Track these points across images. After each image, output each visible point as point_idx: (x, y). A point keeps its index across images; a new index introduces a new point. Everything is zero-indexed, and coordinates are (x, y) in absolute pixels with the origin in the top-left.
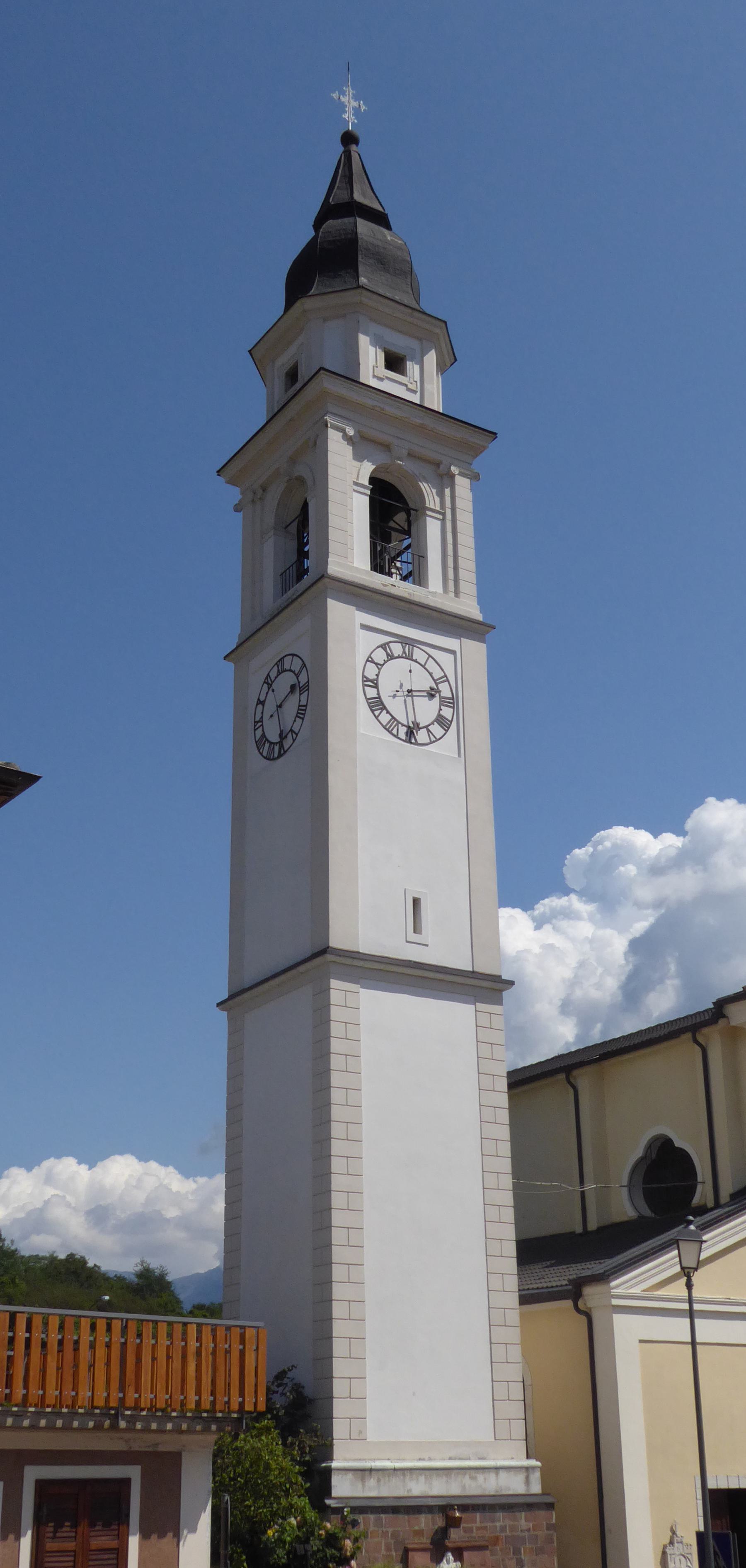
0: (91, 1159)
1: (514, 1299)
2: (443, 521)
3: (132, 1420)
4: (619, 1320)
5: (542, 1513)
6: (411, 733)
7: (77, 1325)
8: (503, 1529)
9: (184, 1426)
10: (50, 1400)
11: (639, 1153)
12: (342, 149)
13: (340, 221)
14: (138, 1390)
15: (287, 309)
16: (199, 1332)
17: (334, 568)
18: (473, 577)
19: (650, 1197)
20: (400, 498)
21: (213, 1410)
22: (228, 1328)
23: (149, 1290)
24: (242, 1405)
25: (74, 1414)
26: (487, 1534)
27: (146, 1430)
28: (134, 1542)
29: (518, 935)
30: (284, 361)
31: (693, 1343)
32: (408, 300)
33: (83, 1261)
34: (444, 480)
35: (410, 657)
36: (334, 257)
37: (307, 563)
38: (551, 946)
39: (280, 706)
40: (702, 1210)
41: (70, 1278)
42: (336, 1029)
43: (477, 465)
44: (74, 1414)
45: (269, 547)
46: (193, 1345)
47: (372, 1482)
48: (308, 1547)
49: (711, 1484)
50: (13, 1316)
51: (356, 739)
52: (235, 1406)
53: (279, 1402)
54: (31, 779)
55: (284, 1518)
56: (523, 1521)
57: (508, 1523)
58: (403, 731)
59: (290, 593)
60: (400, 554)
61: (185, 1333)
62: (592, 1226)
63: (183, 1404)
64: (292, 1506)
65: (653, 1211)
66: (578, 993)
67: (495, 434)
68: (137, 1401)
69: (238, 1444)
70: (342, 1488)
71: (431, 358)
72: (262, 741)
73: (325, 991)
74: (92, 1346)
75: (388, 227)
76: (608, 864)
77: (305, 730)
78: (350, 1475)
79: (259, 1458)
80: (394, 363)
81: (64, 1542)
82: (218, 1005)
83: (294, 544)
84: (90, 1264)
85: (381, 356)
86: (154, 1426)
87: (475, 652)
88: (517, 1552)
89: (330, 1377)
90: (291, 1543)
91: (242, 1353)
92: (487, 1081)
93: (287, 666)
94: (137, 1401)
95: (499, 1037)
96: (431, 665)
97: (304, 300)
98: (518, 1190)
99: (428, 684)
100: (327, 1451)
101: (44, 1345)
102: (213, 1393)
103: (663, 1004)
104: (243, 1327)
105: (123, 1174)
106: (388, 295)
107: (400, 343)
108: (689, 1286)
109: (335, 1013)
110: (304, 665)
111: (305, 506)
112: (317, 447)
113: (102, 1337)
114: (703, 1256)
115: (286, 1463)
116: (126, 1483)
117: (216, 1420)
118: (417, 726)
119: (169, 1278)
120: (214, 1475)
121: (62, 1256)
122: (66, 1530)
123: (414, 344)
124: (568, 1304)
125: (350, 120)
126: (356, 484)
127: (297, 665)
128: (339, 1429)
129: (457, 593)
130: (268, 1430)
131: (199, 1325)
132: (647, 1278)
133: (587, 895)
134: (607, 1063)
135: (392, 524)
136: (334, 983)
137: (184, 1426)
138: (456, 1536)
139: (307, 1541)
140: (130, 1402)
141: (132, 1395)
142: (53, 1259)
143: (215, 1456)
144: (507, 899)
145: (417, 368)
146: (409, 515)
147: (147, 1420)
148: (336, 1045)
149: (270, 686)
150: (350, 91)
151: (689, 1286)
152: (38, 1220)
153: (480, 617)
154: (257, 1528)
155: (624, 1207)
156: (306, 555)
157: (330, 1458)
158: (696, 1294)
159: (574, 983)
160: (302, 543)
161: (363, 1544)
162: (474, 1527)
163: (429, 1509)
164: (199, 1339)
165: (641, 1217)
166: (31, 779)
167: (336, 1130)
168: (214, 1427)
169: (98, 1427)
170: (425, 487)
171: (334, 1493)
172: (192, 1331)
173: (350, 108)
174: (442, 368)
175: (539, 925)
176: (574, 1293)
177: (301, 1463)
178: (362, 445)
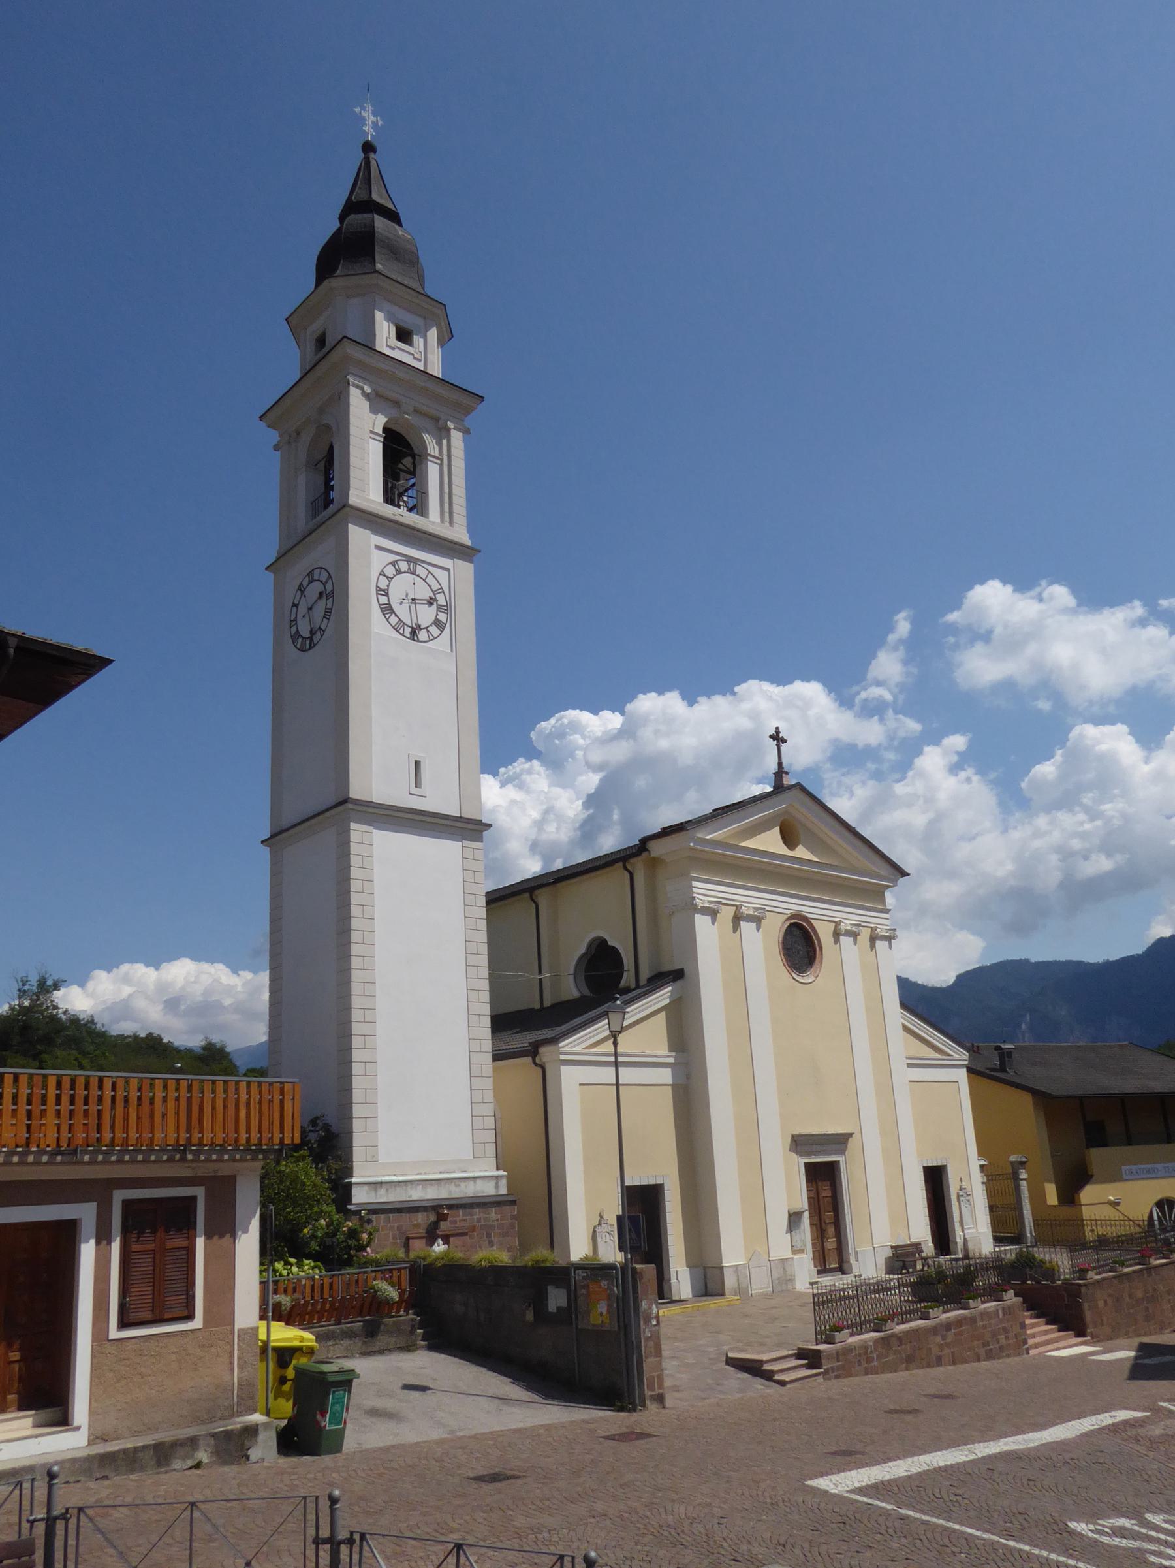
1: (489, 1057)
2: (441, 465)
3: (197, 1154)
5: (507, 1208)
7: (152, 1086)
8: (479, 1220)
9: (238, 1157)
10: (132, 1141)
12: (363, 155)
13: (360, 216)
14: (201, 1132)
15: (316, 287)
16: (248, 1087)
17: (354, 499)
18: (464, 511)
19: (591, 982)
20: (408, 445)
21: (260, 1144)
22: (271, 1084)
23: (213, 1058)
24: (282, 1139)
26: (467, 1224)
27: (208, 1160)
28: (200, 1242)
30: (315, 328)
31: (617, 1085)
33: (160, 1039)
34: (442, 433)
35: (414, 573)
36: (356, 244)
37: (333, 495)
39: (311, 609)
40: (627, 990)
41: (150, 1051)
42: (354, 860)
43: (469, 421)
45: (302, 480)
46: (243, 1097)
47: (382, 1191)
48: (335, 1240)
49: (628, 1183)
50: (101, 1080)
51: (371, 639)
52: (277, 1140)
53: (313, 1137)
54: (105, 662)
55: (317, 1220)
56: (494, 1214)
57: (482, 1215)
58: (408, 631)
59: (318, 519)
60: (407, 490)
61: (237, 1089)
62: (547, 1004)
63: (237, 1140)
64: (322, 1211)
65: (591, 991)
67: (482, 397)
68: (201, 1139)
69: (282, 1168)
70: (359, 1196)
71: (433, 334)
72: (296, 636)
73: (348, 830)
74: (165, 1099)
75: (400, 224)
78: (366, 1188)
79: (298, 1177)
80: (404, 335)
82: (263, 842)
83: (323, 478)
84: (165, 1041)
85: (393, 329)
86: (214, 1157)
87: (464, 570)
88: (489, 1235)
89: (351, 1118)
90: (322, 1238)
91: (282, 1102)
93: (316, 577)
94: (201, 1139)
95: (480, 867)
96: (430, 579)
97: (331, 279)
98: (492, 978)
99: (428, 594)
102: (260, 1132)
103: (609, 842)
104: (282, 1083)
106: (399, 279)
107: (409, 320)
108: (615, 1044)
109: (354, 848)
110: (330, 576)
111: (331, 448)
112: (340, 400)
113: (173, 1094)
114: (626, 1023)
115: (318, 1180)
118: (419, 627)
119: (228, 1050)
120: (262, 1191)
121: (143, 1035)
122: (147, 1235)
123: (419, 321)
124: (529, 1059)
125: (370, 133)
126: (372, 432)
128: (358, 1154)
129: (451, 523)
130: (303, 1158)
131: (249, 1083)
134: (559, 885)
135: (400, 466)
136: (353, 825)
137: (238, 1157)
138: (444, 1226)
139: (334, 1235)
140: (195, 1140)
141: (196, 1136)
142: (136, 1037)
143: (262, 1178)
145: (421, 341)
146: (414, 459)
148: (354, 873)
149: (302, 592)
150: (369, 107)
151: (615, 1044)
153: (469, 543)
154: (297, 1227)
155: (571, 990)
158: (619, 1050)
161: (376, 1236)
163: (425, 1209)
164: (248, 1093)
165: (583, 997)
166: (105, 662)
168: (261, 1156)
169: (170, 1160)
170: (427, 438)
171: (354, 1201)
172: (243, 1086)
173: (370, 123)
174: (442, 343)
175: (503, 784)
176: (533, 1051)
177: (329, 1181)
178: (377, 401)
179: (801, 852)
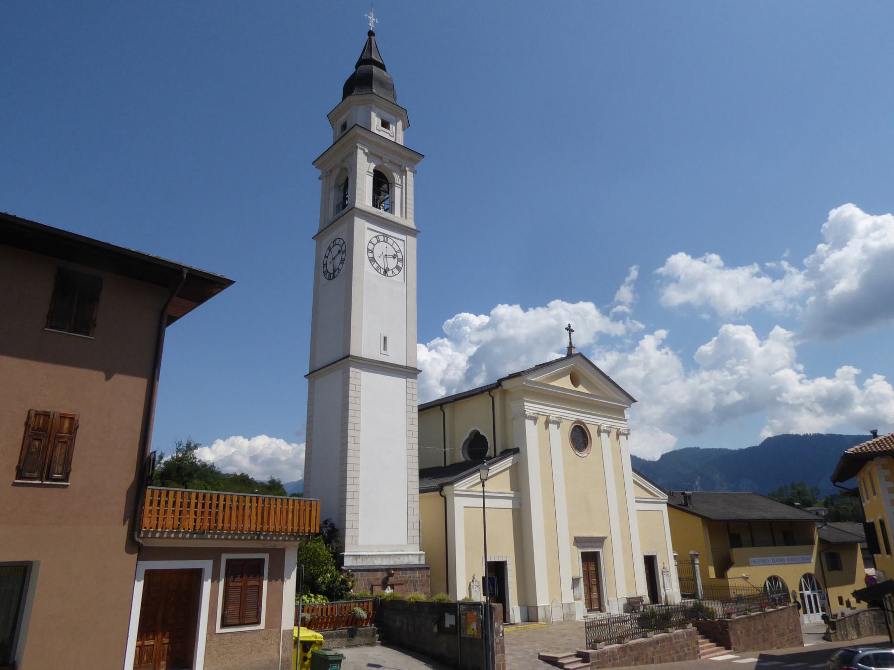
0: (249, 437)
4: (456, 499)
5: (424, 571)
6: (385, 272)
11: (467, 436)
14: (268, 524)
17: (358, 205)
19: (470, 453)
21: (298, 532)
23: (274, 487)
25: (242, 534)
27: (271, 540)
28: (265, 583)
29: (423, 355)
30: (341, 121)
31: (484, 507)
32: (392, 100)
34: (403, 173)
36: (363, 80)
37: (347, 202)
38: (435, 359)
40: (489, 458)
41: (242, 482)
43: (416, 167)
44: (242, 534)
45: (332, 195)
46: (291, 507)
47: (360, 560)
49: (488, 560)
51: (363, 273)
52: (307, 530)
56: (417, 574)
58: (382, 271)
62: (448, 464)
66: (447, 377)
70: (348, 562)
71: (400, 124)
75: (385, 70)
76: (458, 326)
77: (344, 269)
80: (385, 124)
81: (238, 583)
83: (342, 194)
85: (380, 121)
87: (412, 241)
88: (415, 585)
91: (310, 511)
92: (410, 409)
95: (415, 392)
96: (395, 245)
100: (342, 548)
101: (231, 508)
103: (480, 381)
105: (262, 443)
107: (388, 117)
108: (483, 486)
111: (347, 180)
112: (353, 155)
115: (327, 553)
116: (263, 560)
117: (299, 536)
121: (239, 474)
122: (238, 579)
123: (394, 118)
125: (372, 26)
127: (341, 243)
128: (348, 540)
129: (406, 217)
130: (319, 540)
132: (467, 484)
133: (450, 339)
136: (351, 369)
138: (392, 580)
140: (265, 529)
141: (266, 527)
142: (235, 475)
144: (419, 342)
147: (272, 537)
148: (351, 393)
151: (483, 486)
152: (229, 460)
153: (414, 228)
154: (314, 577)
155: (461, 457)
156: (347, 199)
157: (344, 551)
159: (445, 372)
160: (345, 194)
161: (356, 583)
162: (399, 577)
163: (382, 570)
164: (293, 505)
167: (350, 426)
169: (252, 539)
170: (395, 175)
173: (372, 22)
174: (404, 128)
175: (430, 350)
176: (440, 489)
178: (371, 156)
179: (581, 388)
